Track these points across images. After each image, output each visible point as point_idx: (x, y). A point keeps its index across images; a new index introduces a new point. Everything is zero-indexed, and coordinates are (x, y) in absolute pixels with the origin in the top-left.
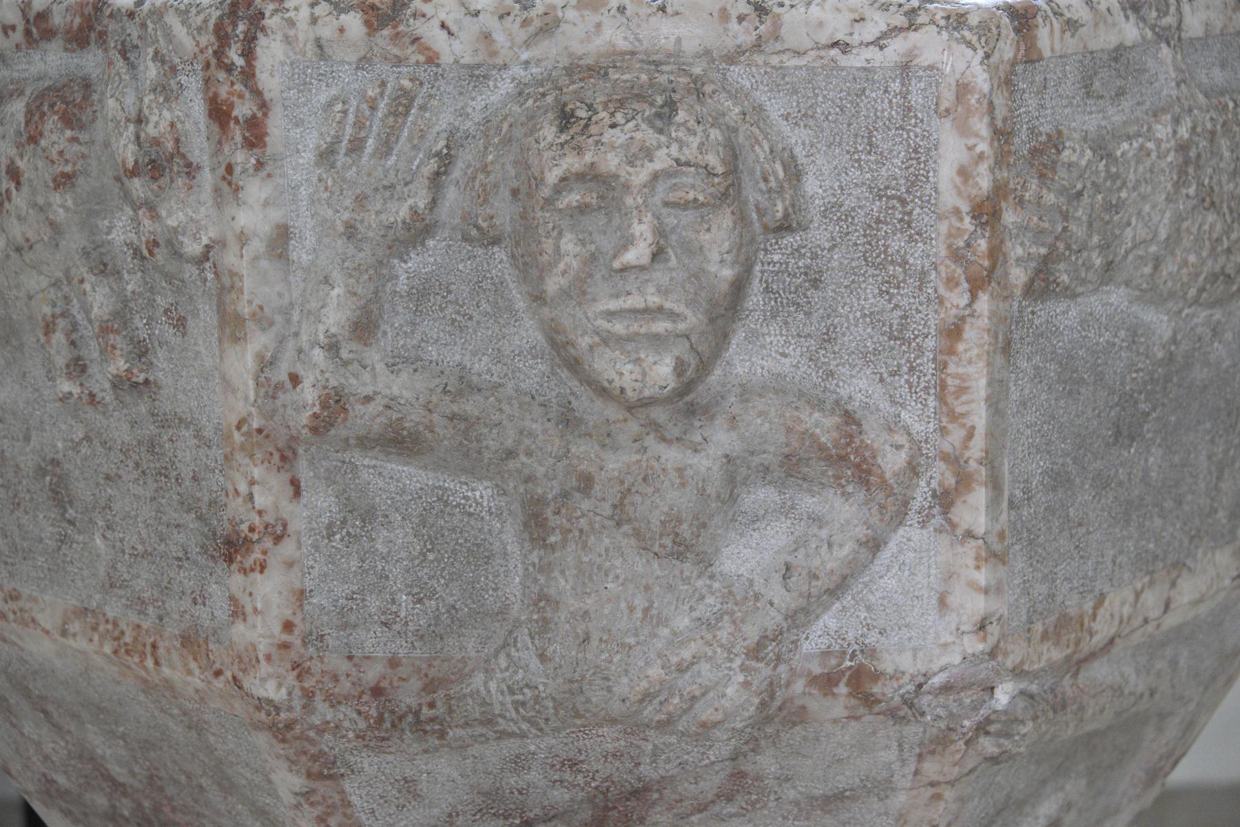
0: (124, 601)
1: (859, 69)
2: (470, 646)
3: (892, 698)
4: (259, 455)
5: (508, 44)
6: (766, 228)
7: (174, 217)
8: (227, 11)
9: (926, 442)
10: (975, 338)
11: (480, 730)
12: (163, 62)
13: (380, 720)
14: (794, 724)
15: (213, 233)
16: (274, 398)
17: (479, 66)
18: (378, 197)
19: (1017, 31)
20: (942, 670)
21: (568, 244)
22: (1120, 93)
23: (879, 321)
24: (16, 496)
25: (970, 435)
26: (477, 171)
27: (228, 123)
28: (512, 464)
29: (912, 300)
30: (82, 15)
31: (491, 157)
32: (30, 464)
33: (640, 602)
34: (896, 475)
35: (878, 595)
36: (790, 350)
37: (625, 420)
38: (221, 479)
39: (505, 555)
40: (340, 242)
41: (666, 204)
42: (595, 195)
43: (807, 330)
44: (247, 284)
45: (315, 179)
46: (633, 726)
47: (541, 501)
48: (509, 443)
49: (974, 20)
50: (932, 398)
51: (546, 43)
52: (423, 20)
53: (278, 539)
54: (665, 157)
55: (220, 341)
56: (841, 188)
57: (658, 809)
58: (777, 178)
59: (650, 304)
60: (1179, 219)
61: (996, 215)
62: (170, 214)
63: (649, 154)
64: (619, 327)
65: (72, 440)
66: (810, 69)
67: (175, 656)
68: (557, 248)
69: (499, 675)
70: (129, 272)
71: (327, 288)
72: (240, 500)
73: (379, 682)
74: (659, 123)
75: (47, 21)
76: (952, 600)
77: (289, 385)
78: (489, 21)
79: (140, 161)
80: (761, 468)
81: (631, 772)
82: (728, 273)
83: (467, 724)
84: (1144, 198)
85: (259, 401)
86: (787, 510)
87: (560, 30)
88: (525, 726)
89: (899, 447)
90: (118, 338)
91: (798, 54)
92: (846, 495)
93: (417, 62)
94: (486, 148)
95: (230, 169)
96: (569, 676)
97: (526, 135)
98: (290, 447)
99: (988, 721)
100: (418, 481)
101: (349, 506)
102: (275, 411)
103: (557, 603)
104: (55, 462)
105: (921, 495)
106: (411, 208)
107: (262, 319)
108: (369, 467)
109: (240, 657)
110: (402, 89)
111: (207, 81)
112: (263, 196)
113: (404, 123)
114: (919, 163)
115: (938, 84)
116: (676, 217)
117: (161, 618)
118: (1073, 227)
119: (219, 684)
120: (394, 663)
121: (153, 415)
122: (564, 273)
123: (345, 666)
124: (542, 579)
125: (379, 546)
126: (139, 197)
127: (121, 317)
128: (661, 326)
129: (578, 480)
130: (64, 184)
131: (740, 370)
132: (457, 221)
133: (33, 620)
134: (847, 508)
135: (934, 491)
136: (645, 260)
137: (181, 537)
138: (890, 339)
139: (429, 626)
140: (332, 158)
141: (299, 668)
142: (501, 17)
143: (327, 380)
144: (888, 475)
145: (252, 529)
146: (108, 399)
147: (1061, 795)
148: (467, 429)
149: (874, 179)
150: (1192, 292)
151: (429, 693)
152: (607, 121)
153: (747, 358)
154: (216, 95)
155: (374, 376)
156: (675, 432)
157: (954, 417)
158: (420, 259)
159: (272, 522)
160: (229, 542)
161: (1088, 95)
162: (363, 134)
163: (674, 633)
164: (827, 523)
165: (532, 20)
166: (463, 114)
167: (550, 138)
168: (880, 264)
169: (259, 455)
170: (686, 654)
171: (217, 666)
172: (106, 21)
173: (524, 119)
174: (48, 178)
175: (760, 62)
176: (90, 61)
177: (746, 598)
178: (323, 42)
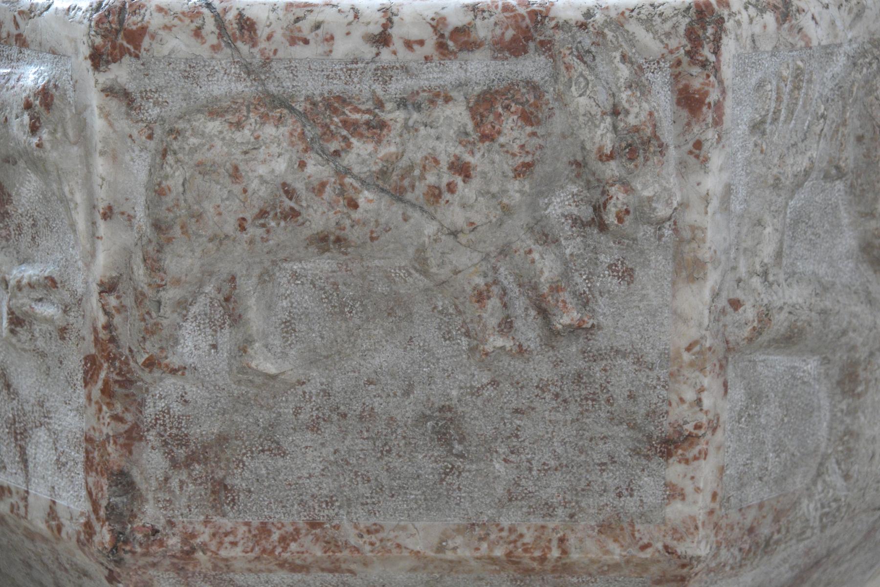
7: (651, 189)
8: (695, 18)
12: (632, 63)
17: (830, 45)
24: (386, 444)
27: (700, 108)
28: (844, 340)
38: (664, 393)
40: (768, 192)
44: (709, 234)
45: (751, 146)
53: (714, 430)
55: (674, 283)
62: (645, 186)
65: (472, 387)
67: (589, 544)
71: (759, 228)
72: (685, 406)
75: (469, 36)
77: (729, 309)
95: (698, 145)
111: (676, 77)
117: (572, 516)
124: (848, 420)
132: (825, 164)
133: (399, 546)
137: (610, 446)
145: (698, 427)
146: (532, 346)
154: (686, 87)
159: (712, 418)
171: (646, 541)
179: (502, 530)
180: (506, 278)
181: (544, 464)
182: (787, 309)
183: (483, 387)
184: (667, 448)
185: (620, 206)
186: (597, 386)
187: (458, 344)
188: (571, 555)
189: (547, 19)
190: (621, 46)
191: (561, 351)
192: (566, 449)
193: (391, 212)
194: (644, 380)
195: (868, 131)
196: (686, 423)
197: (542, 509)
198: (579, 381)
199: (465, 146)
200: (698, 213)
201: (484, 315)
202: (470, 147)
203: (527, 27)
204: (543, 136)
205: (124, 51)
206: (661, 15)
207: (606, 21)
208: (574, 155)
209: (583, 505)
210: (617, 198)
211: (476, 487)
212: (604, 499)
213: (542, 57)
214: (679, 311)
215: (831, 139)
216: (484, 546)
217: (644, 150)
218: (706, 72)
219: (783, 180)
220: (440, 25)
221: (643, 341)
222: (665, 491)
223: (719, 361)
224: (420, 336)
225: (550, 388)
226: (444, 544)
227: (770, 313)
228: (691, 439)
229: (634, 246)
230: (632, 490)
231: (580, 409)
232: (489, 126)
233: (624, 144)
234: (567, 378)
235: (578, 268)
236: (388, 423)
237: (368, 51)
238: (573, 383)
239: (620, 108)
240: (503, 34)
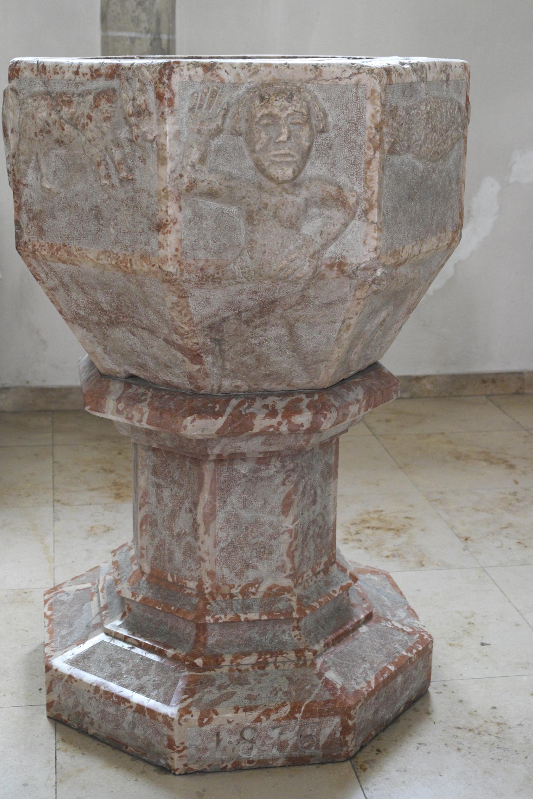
6: (317, 131)
10: (375, 164)
11: (231, 281)
12: (141, 82)
13: (202, 278)
14: (321, 279)
15: (157, 133)
17: (236, 83)
19: (387, 75)
20: (364, 263)
21: (263, 135)
22: (412, 96)
25: (373, 193)
28: (244, 201)
30: (112, 69)
31: (240, 110)
32: (87, 208)
33: (280, 241)
34: (353, 204)
35: (346, 240)
36: (323, 168)
39: (240, 228)
41: (291, 123)
43: (328, 162)
45: (188, 117)
46: (275, 279)
47: (252, 212)
49: (376, 71)
53: (175, 224)
55: (158, 165)
57: (278, 307)
60: (426, 134)
61: (381, 128)
62: (143, 127)
63: (286, 108)
64: (278, 159)
66: (330, 85)
67: (138, 262)
68: (260, 136)
72: (163, 212)
74: (289, 100)
77: (179, 178)
81: (272, 295)
82: (307, 144)
84: (418, 127)
86: (321, 215)
88: (244, 280)
89: (354, 196)
91: (327, 81)
92: (338, 210)
95: (163, 113)
99: (375, 279)
104: (97, 207)
105: (359, 211)
109: (161, 260)
110: (214, 90)
111: (156, 88)
115: (366, 90)
117: (133, 251)
118: (400, 134)
119: (154, 269)
120: (207, 261)
122: (261, 143)
123: (192, 262)
124: (251, 235)
125: (204, 226)
127: (124, 159)
128: (289, 159)
133: (87, 256)
136: (286, 139)
137: (142, 226)
141: (180, 263)
142: (242, 69)
145: (167, 221)
147: (387, 310)
149: (347, 117)
150: (429, 157)
152: (274, 99)
154: (159, 92)
155: (205, 174)
157: (369, 188)
160: (158, 226)
161: (404, 96)
163: (290, 251)
167: (258, 104)
170: (293, 257)
171: (153, 263)
172: (120, 71)
174: (102, 118)
176: (115, 83)
183: (106, 200)
193: (74, 133)
205: (15, 76)
212: (141, 246)
216: (110, 259)
219: (202, 131)
223: (176, 197)
228: (165, 225)
237: (73, 77)
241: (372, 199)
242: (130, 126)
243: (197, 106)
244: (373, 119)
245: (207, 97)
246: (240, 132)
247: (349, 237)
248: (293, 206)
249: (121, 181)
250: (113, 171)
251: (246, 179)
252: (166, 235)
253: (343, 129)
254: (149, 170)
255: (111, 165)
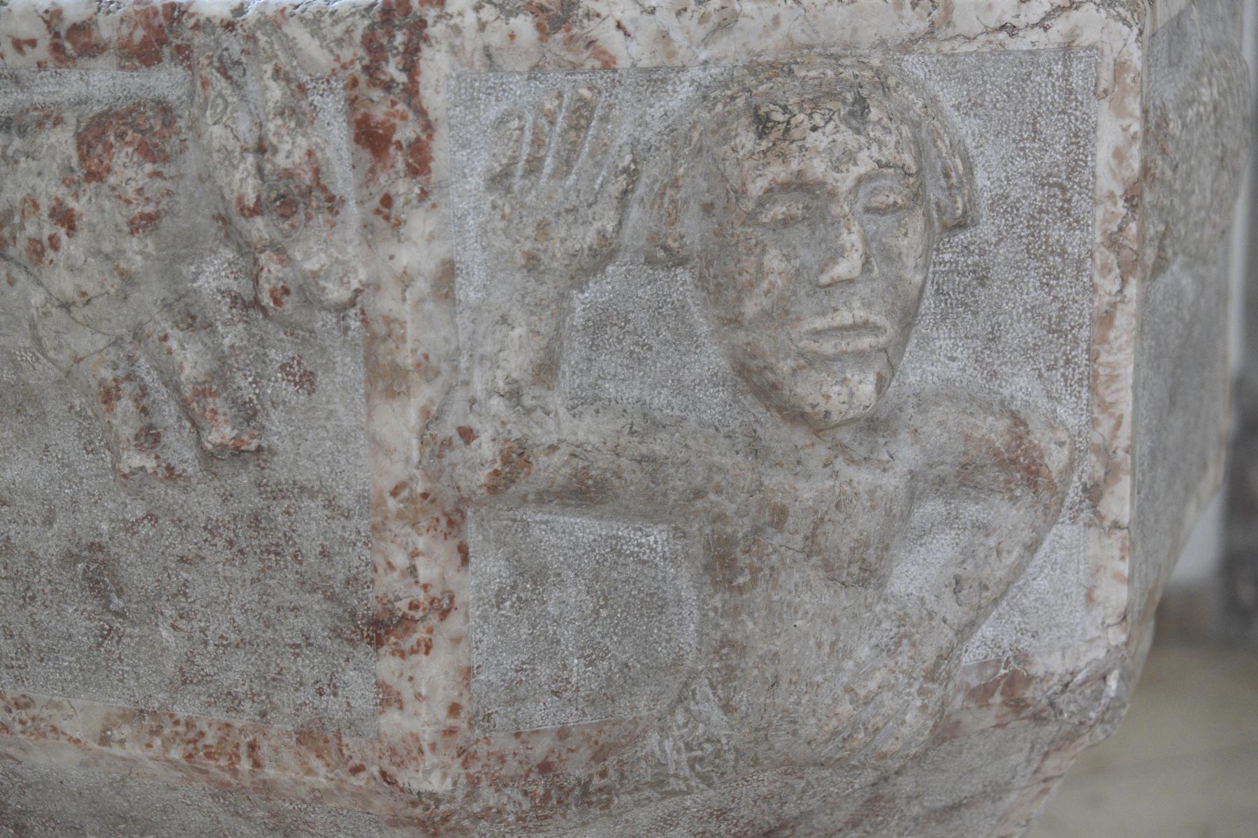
0: (203, 698)
1: (1024, 52)
2: (642, 704)
3: (1040, 701)
4: (424, 523)
5: (686, 43)
7: (314, 260)
8: (378, 19)
9: (1079, 435)
10: (1125, 321)
11: (647, 793)
13: (547, 796)
14: (944, 740)
15: (363, 275)
16: (440, 456)
17: (657, 69)
18: (561, 222)
23: (1039, 314)
24: (28, 588)
25: (1118, 425)
26: (665, 187)
27: (386, 149)
28: (699, 504)
29: (1069, 291)
30: (148, 26)
31: (681, 170)
33: (827, 637)
35: (1032, 597)
36: (957, 354)
37: (813, 445)
38: (367, 552)
40: (518, 276)
41: (868, 210)
42: (801, 206)
44: (410, 330)
45: (487, 207)
47: (730, 541)
48: (698, 481)
50: (1085, 389)
51: (725, 39)
52: (598, 20)
53: (444, 614)
54: (867, 159)
55: (368, 397)
56: (1007, 178)
58: (957, 173)
59: (858, 319)
62: (308, 256)
63: (850, 157)
64: (828, 347)
65: (125, 520)
66: (978, 54)
67: (287, 757)
69: (676, 733)
70: (224, 324)
71: (505, 328)
72: (396, 575)
73: (547, 757)
74: (854, 122)
75: (90, 36)
76: (1098, 594)
77: (458, 441)
78: (665, 18)
79: (264, 196)
80: (937, 481)
83: (636, 789)
85: (425, 462)
86: (950, 521)
87: (738, 25)
90: (217, 401)
91: (969, 39)
92: (1014, 500)
93: (593, 68)
94: (674, 160)
95: (387, 201)
96: (755, 725)
97: (718, 144)
98: (458, 510)
100: (591, 533)
101: (519, 569)
102: (441, 471)
103: (745, 647)
105: (1073, 493)
106: (599, 232)
107: (426, 369)
108: (541, 522)
110: (581, 99)
111: (352, 102)
112: (428, 229)
113: (585, 138)
114: (1079, 148)
116: (875, 223)
117: (263, 714)
119: (359, 781)
120: (563, 734)
121: (259, 486)
122: (767, 293)
123: (511, 745)
124: (726, 625)
125: (550, 609)
126: (261, 239)
127: (220, 374)
128: (866, 342)
129: (772, 515)
130: (145, 227)
131: (912, 379)
133: (54, 729)
134: (1015, 512)
135: (1084, 485)
136: (856, 273)
137: (301, 622)
138: (1049, 332)
139: (601, 689)
140: (506, 183)
142: (678, 14)
143: (509, 432)
144: (1054, 474)
145: (414, 606)
146: (190, 470)
148: (655, 470)
151: (598, 762)
152: (807, 124)
153: (918, 365)
155: (558, 424)
156: (861, 452)
157: (1105, 407)
158: (597, 287)
159: (438, 596)
160: (375, 623)
162: (542, 153)
164: (994, 530)
165: (710, 15)
166: (642, 123)
167: (749, 146)
168: (1041, 255)
169: (424, 523)
170: (873, 685)
172: (188, 34)
173: (714, 125)
175: (933, 51)
177: (922, 618)
178: (492, 50)
179: (177, 723)
180: (148, 373)
181: (222, 637)
182: (564, 449)
183: (139, 521)
184: (375, 632)
185: (273, 282)
186: (280, 535)
187: (102, 459)
188: (266, 770)
189: (185, 16)
190: (276, 56)
191: (229, 482)
192: (248, 620)
194: (339, 533)
195: (718, 197)
196: (398, 599)
197: (225, 700)
198: (257, 526)
199: (68, 186)
200: (393, 299)
201: (114, 422)
202: (74, 188)
203: (160, 26)
204: (172, 178)
206: (333, 13)
207: (259, 20)
208: (216, 207)
209: (275, 700)
210: (269, 271)
211: (140, 660)
212: (301, 697)
213: (180, 68)
214: (378, 438)
215: (652, 207)
216: (158, 742)
217: (305, 204)
218: (392, 97)
220: (55, 20)
221: (333, 476)
222: (378, 693)
224: (56, 444)
225: (221, 530)
226: (109, 733)
227: (527, 452)
229: (312, 340)
230: (335, 686)
231: (260, 565)
232: (96, 161)
233: (273, 195)
234: (241, 520)
235: (241, 367)
236: (29, 560)
238: (250, 527)
239: (266, 144)
240: (131, 34)
241: (1115, 444)
242: (247, 249)
243: (521, 165)
244: (1120, 163)
245: (558, 130)
246: (683, 253)
247: (1041, 584)
248: (873, 507)
249: (208, 457)
250: (168, 414)
251: (700, 423)
252: (413, 659)
253: (1025, 209)
254: (331, 414)
255: (160, 393)
